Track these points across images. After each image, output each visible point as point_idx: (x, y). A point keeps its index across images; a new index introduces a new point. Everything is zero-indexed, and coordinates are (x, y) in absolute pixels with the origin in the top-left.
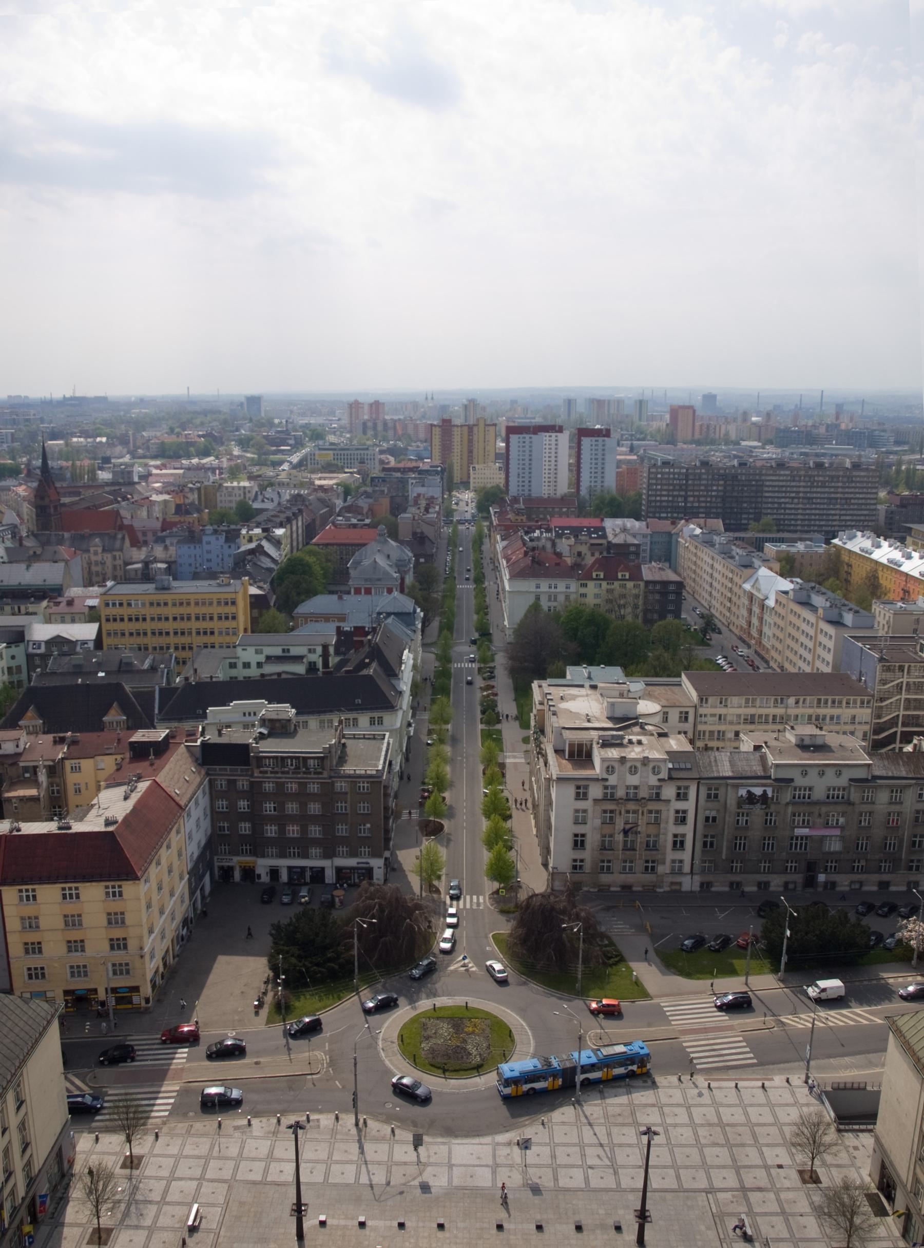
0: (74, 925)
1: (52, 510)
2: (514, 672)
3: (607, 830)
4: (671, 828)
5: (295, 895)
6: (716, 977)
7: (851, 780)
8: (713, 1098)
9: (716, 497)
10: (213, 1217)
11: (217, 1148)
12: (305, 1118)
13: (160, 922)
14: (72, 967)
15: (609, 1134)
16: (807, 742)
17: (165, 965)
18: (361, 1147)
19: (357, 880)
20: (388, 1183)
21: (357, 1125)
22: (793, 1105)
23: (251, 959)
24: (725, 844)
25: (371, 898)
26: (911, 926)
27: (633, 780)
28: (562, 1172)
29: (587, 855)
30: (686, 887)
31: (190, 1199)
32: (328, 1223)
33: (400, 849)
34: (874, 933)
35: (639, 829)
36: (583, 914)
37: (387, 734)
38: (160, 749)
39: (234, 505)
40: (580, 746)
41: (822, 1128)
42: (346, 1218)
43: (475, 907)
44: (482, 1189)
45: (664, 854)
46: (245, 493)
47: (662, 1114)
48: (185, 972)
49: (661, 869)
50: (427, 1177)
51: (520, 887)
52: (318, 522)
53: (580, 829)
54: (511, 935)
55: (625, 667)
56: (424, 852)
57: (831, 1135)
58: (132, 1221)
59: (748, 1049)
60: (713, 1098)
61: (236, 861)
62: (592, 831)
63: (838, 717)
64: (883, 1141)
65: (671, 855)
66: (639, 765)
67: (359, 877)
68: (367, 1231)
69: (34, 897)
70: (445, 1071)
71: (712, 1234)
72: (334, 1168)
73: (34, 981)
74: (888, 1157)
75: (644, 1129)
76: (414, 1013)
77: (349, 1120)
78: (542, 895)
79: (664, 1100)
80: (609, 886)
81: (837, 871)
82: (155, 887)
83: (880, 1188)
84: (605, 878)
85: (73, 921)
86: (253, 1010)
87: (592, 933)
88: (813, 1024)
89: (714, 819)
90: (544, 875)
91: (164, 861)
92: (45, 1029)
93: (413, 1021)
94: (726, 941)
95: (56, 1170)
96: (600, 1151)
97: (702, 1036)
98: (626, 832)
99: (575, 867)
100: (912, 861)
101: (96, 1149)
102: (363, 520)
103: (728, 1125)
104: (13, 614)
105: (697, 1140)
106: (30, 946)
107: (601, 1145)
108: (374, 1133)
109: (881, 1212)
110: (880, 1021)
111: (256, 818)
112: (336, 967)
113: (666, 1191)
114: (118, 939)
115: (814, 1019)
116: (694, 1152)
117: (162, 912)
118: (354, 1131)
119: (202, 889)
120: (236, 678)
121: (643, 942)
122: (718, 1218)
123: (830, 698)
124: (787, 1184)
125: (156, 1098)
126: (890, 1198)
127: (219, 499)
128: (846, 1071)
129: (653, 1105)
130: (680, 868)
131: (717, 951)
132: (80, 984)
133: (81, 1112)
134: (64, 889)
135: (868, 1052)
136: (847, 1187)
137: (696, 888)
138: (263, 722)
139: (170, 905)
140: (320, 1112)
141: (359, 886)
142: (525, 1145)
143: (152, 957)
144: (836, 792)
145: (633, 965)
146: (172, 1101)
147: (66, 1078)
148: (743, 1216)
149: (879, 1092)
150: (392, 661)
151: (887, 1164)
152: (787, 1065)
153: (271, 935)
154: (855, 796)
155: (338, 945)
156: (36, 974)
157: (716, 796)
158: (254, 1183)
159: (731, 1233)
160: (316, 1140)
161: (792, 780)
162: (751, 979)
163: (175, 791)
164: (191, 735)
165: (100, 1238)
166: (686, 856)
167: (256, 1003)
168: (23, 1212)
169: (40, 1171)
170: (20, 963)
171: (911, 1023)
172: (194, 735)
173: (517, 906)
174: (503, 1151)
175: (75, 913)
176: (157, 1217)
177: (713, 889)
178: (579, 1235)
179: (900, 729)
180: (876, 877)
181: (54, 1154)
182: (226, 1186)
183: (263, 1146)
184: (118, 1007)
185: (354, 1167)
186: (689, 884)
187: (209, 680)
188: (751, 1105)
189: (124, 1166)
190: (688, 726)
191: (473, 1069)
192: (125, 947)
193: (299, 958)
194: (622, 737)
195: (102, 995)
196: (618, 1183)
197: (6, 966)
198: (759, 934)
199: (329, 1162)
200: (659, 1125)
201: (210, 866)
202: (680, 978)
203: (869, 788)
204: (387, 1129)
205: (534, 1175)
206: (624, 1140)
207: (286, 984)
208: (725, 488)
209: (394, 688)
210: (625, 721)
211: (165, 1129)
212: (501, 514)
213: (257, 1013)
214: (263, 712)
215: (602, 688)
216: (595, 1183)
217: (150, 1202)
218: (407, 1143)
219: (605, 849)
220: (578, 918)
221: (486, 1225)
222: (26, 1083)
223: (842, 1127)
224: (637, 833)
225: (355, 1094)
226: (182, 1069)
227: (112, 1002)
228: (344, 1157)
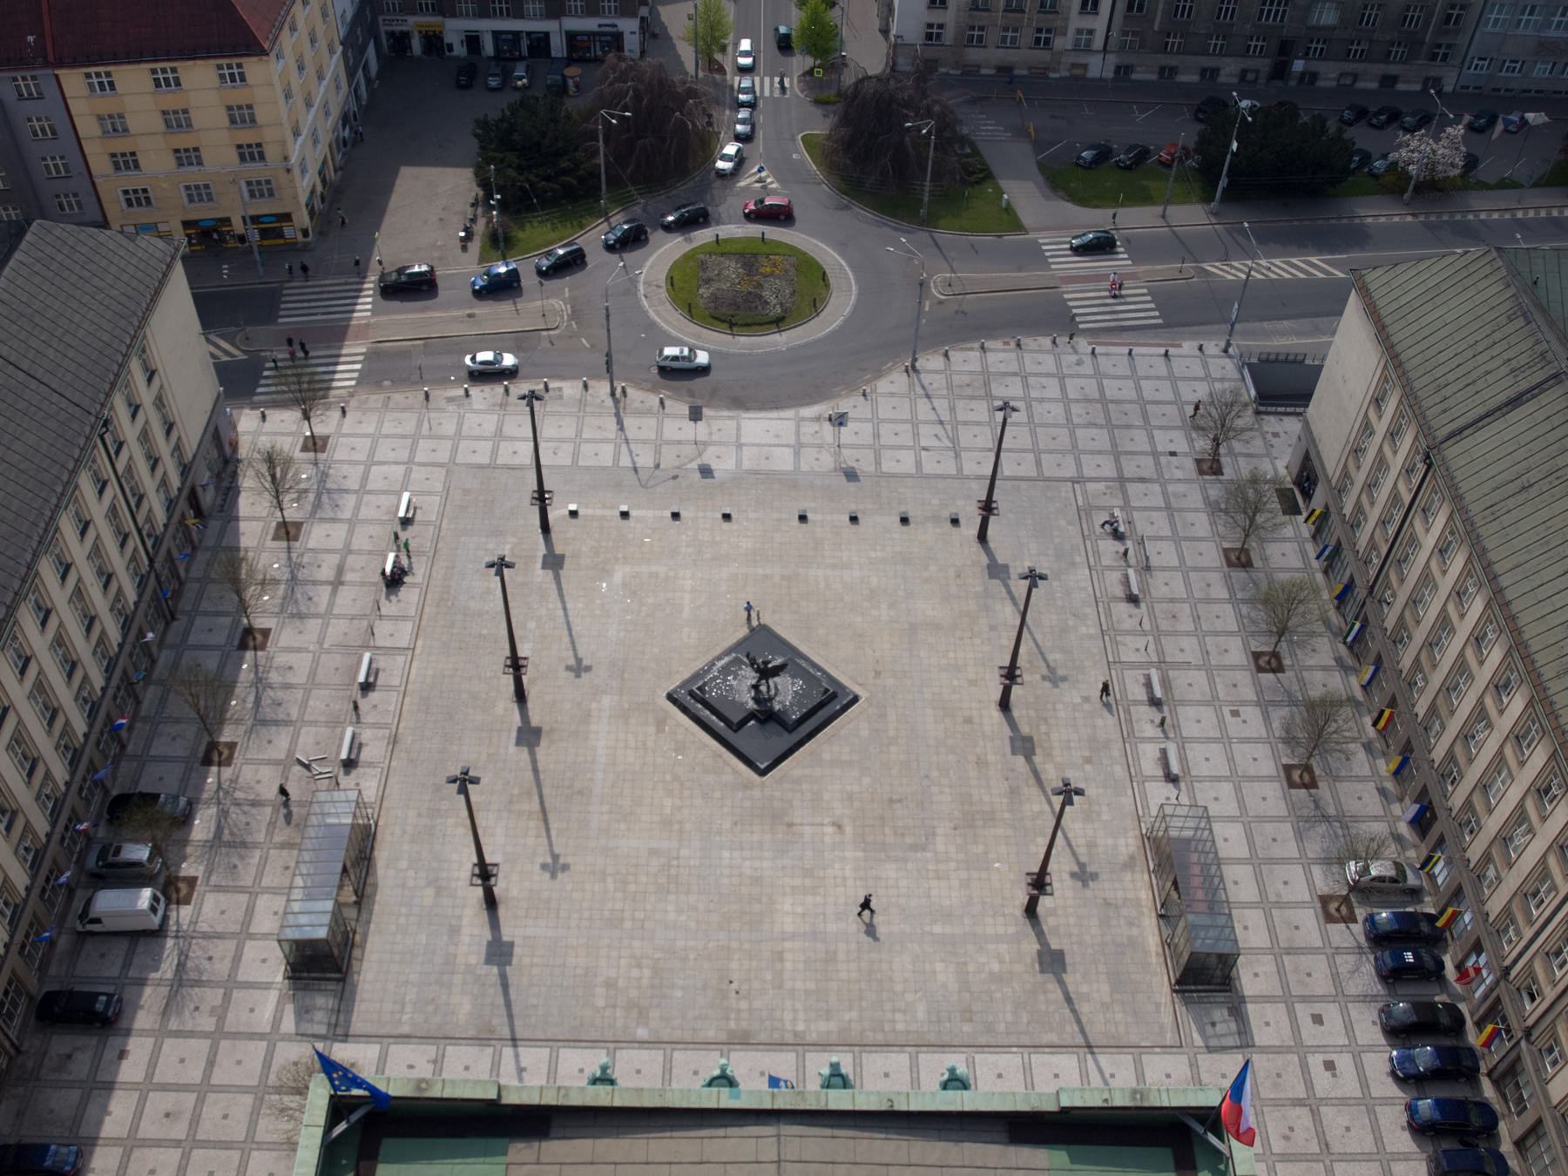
5: (507, 77)
6: (1122, 205)
8: (1096, 367)
10: (430, 509)
11: (426, 425)
12: (542, 386)
13: (308, 119)
14: (188, 188)
15: (952, 409)
17: (324, 181)
18: (620, 423)
19: (599, 53)
20: (657, 466)
21: (613, 394)
22: (1202, 379)
23: (448, 170)
24: (1161, 6)
25: (622, 78)
26: (1414, 144)
28: (886, 454)
31: (398, 487)
32: (581, 512)
33: (664, 4)
34: (1360, 151)
36: (937, 108)
41: (1236, 409)
42: (604, 507)
43: (777, 94)
44: (781, 473)
45: (1067, 19)
47: (1026, 386)
48: (352, 194)
49: (1059, 43)
50: (708, 457)
51: (845, 65)
54: (829, 137)
56: (701, 8)
57: (1247, 418)
58: (328, 513)
60: (1096, 367)
64: (1313, 428)
67: (602, 48)
68: (631, 523)
69: (111, 84)
70: (732, 325)
71: (1074, 530)
72: (585, 448)
73: (135, 209)
74: (1316, 446)
75: (1000, 403)
76: (687, 248)
77: (601, 389)
78: (878, 78)
79: (1030, 367)
80: (979, 66)
81: (1323, 56)
82: (293, 66)
83: (1298, 482)
84: (974, 55)
85: (178, 120)
86: (459, 244)
87: (948, 136)
88: (1249, 275)
90: (882, 48)
91: (300, 24)
92: (165, 275)
93: (687, 257)
94: (1143, 154)
95: (215, 455)
96: (939, 430)
97: (1091, 286)
99: (929, 36)
100: (1439, 46)
101: (264, 429)
103: (1112, 401)
105: (1069, 419)
107: (941, 422)
108: (637, 404)
109: (1292, 509)
110: (1341, 275)
112: (574, 182)
113: (1022, 479)
114: (249, 146)
115: (1251, 269)
116: (1063, 433)
117: (309, 105)
118: (609, 402)
119: (366, 68)
121: (1022, 152)
122: (1084, 512)
124: (1179, 474)
125: (337, 364)
126: (1307, 495)
128: (1283, 339)
129: (1015, 374)
130: (1089, 42)
131: (1129, 168)
132: (204, 212)
133: (238, 382)
134: (154, 71)
135: (1317, 316)
136: (1254, 480)
137: (1109, 74)
140: (562, 378)
141: (603, 62)
142: (839, 420)
143: (304, 171)
145: (1003, 184)
146: (358, 366)
147: (208, 340)
148: (1117, 513)
149: (1321, 367)
151: (1313, 455)
152: (1203, 328)
153: (476, 136)
155: (576, 149)
158: (480, 467)
159: (1099, 530)
160: (559, 414)
162: (1171, 210)
165: (288, 533)
167: (462, 234)
168: (183, 505)
169: (194, 456)
170: (112, 186)
171: (1385, 279)
173: (839, 94)
174: (809, 429)
175: (179, 107)
176: (357, 508)
177: (1134, 76)
178: (905, 528)
180: (1379, 69)
181: (209, 436)
182: (443, 471)
183: (490, 423)
184: (265, 243)
185: (611, 447)
186: (1099, 67)
188: (1147, 378)
189: (305, 449)
191: (771, 323)
192: (262, 157)
193: (520, 169)
195: (238, 227)
196: (960, 469)
197: (91, 190)
198: (1191, 145)
199: (578, 440)
200: (1019, 399)
202: (1069, 205)
204: (653, 400)
205: (849, 458)
206: (971, 417)
207: (503, 205)
211: (353, 403)
213: (464, 248)
216: (928, 468)
217: (347, 491)
218: (682, 417)
219: (977, 9)
220: (929, 113)
221: (784, 516)
223: (1262, 409)
225: (609, 355)
226: (367, 325)
227: (254, 236)
228: (598, 435)
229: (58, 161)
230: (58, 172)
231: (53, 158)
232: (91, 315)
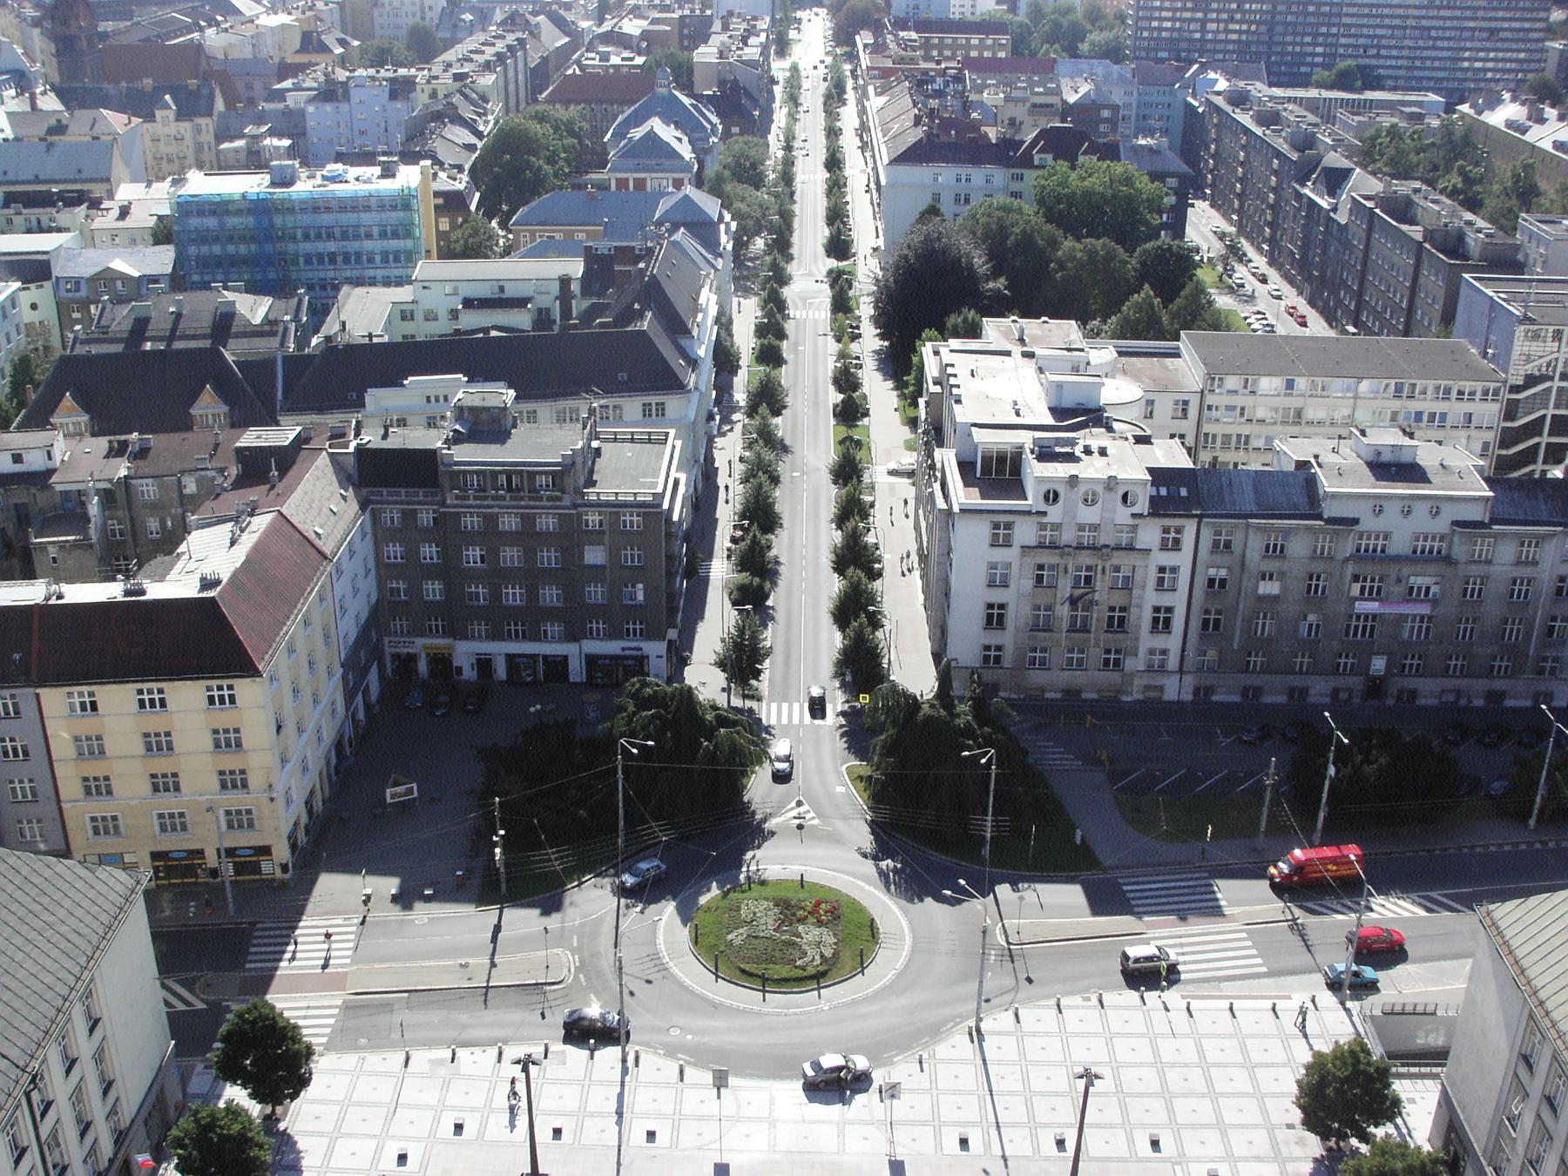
0: (160, 749)
1: (85, 44)
2: (887, 321)
3: (1043, 597)
4: (1149, 598)
7: (1456, 523)
9: (1258, 23)
12: (542, 1049)
14: (161, 816)
16: (1386, 457)
17: (310, 812)
21: (624, 1061)
24: (1239, 623)
27: (1089, 515)
29: (1007, 638)
30: (1171, 694)
35: (1097, 597)
37: (672, 432)
38: (286, 460)
39: (403, 32)
40: (1001, 458)
45: (1137, 639)
46: (423, 12)
49: (1130, 664)
52: (551, 66)
53: (997, 596)
55: (1083, 320)
59: (1254, 952)
61: (420, 645)
62: (1018, 598)
63: (1443, 416)
65: (1147, 641)
66: (1100, 489)
80: (1043, 690)
85: (159, 744)
89: (1223, 582)
98: (1073, 601)
100: (1545, 659)
102: (632, 59)
104: (29, 231)
106: (93, 784)
111: (448, 569)
119: (366, 693)
120: (413, 336)
123: (1431, 384)
127: (378, 20)
132: (175, 843)
138: (460, 412)
139: (312, 719)
144: (1428, 544)
146: (332, 1021)
147: (164, 986)
150: (680, 305)
154: (1459, 551)
156: (105, 826)
157: (1228, 545)
161: (1355, 521)
163: (311, 526)
164: (338, 436)
166: (1173, 642)
169: (133, 1121)
170: (79, 811)
172: (343, 435)
175: (162, 731)
177: (1215, 698)
179: (1545, 439)
180: (1481, 685)
187: (366, 341)
190: (1188, 426)
192: (245, 785)
194: (1072, 443)
195: (212, 860)
197: (57, 816)
201: (377, 654)
203: (1483, 536)
208: (1273, 17)
209: (683, 353)
210: (1080, 413)
212: (878, 48)
214: (460, 395)
215: (1044, 357)
218: (704, 1086)
222: (101, 993)
224: (1092, 603)
227: (229, 870)
229: (27, 785)
230: (24, 796)
231: (21, 781)
232: (35, 953)
